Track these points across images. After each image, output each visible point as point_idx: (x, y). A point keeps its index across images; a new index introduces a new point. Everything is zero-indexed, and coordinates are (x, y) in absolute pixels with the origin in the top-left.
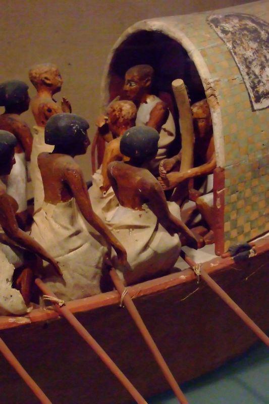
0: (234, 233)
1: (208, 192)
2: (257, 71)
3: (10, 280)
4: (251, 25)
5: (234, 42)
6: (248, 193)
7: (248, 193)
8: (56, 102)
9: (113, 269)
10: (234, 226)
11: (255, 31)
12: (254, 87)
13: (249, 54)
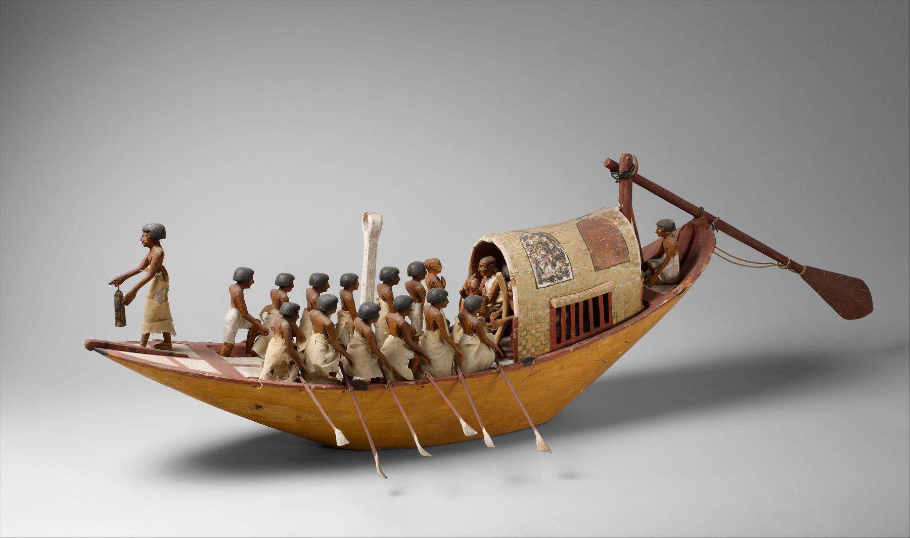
0: (524, 353)
1: (614, 322)
2: (542, 267)
3: (559, 365)
4: (545, 240)
5: (532, 251)
6: (533, 331)
7: (533, 331)
8: (93, 346)
9: (423, 366)
10: (524, 348)
11: (547, 244)
12: (539, 276)
13: (539, 257)
